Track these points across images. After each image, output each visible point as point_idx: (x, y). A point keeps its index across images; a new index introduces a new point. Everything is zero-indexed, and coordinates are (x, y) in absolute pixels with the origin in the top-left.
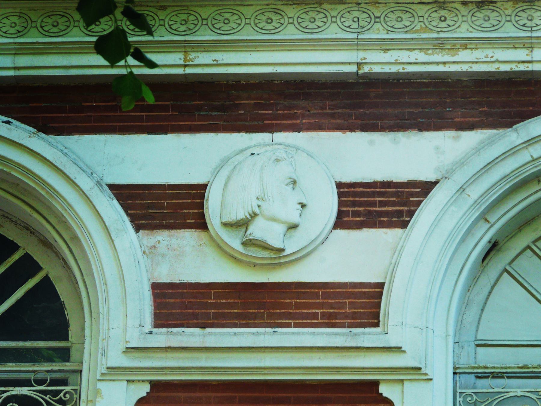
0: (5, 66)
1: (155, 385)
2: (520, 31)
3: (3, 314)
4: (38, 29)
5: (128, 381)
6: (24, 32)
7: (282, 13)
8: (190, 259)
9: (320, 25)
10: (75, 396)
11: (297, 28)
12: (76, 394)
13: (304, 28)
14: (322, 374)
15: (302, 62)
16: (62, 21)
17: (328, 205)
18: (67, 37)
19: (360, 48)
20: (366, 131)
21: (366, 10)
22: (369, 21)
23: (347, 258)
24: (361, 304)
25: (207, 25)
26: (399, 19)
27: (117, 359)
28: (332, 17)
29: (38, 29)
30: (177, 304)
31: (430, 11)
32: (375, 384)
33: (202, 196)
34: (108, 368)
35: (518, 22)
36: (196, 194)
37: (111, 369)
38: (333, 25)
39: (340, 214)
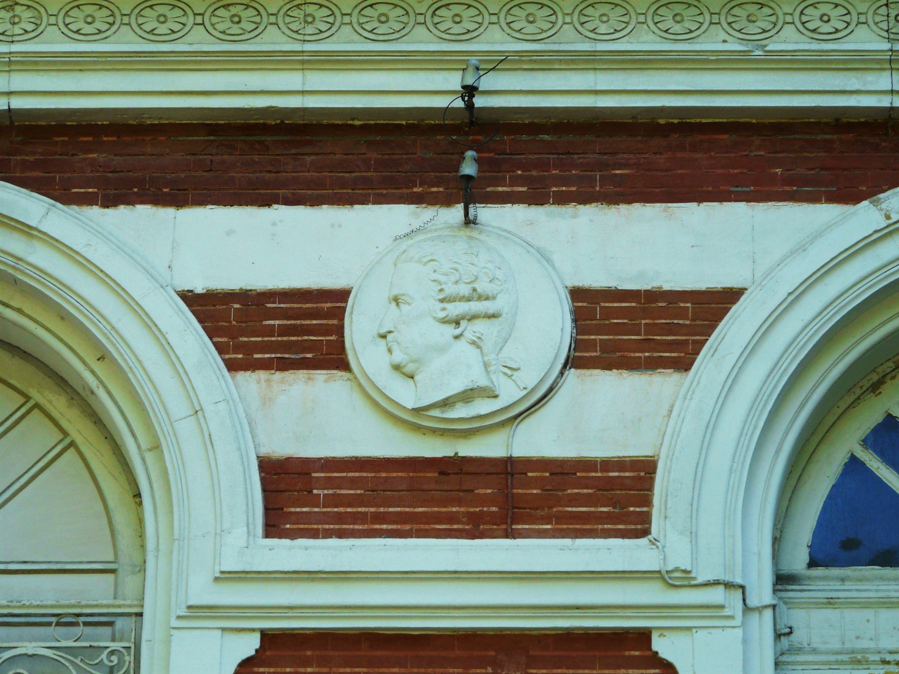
0: (65, 90)
1: (269, 638)
2: (218, 41)
5: (223, 629)
6: (108, 33)
7: (628, 7)
8: (322, 419)
9: (29, 29)
10: (127, 658)
11: (356, 31)
12: (129, 655)
13: (75, 32)
14: (592, 617)
15: (828, 89)
16: (394, 13)
17: (554, 328)
18: (36, 43)
19: (13, 67)
23: (599, 416)
24: (610, 496)
25: (129, 24)
26: (383, 19)
27: (202, 590)
30: (293, 494)
32: (643, 637)
33: (340, 314)
34: (190, 607)
36: (329, 305)
37: (197, 611)
39: (577, 344)
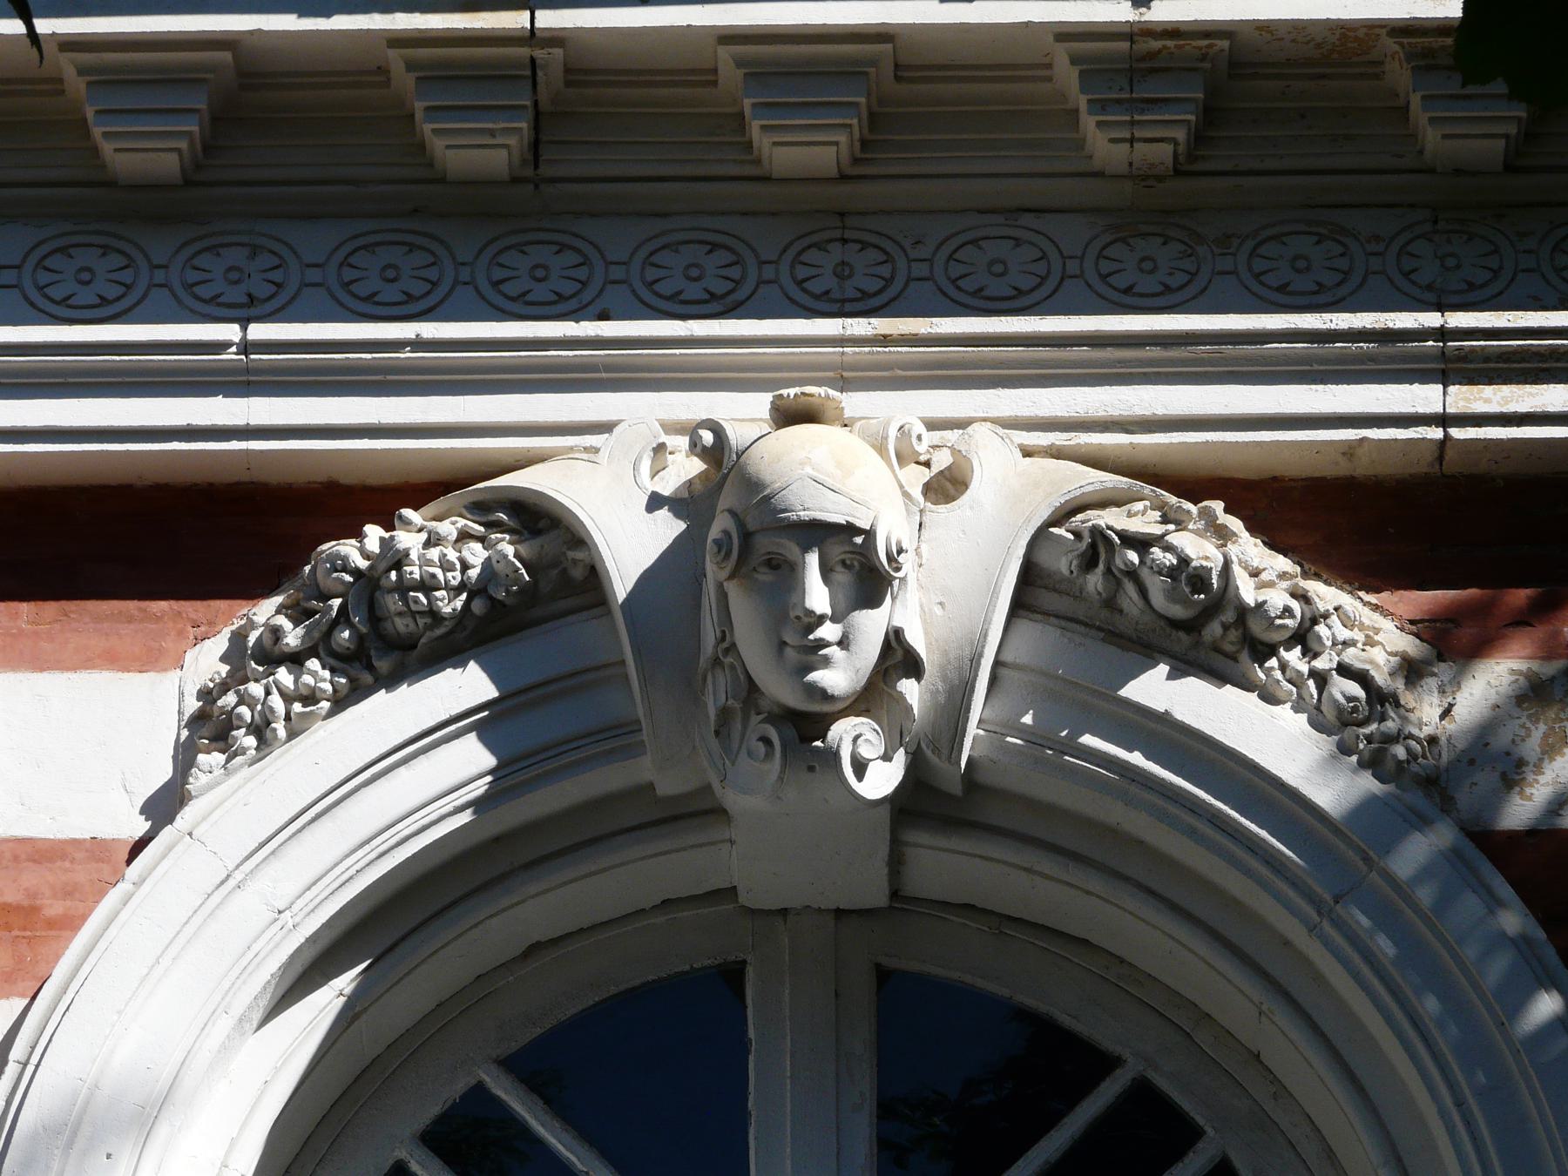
3: (606, 1153)
4: (175, 295)
9: (416, 292)
20: (42, 670)
21: (419, 240)
22: (888, 275)
28: (609, 264)
29: (175, 295)
31: (45, 249)
35: (1110, 279)
38: (156, 293)
